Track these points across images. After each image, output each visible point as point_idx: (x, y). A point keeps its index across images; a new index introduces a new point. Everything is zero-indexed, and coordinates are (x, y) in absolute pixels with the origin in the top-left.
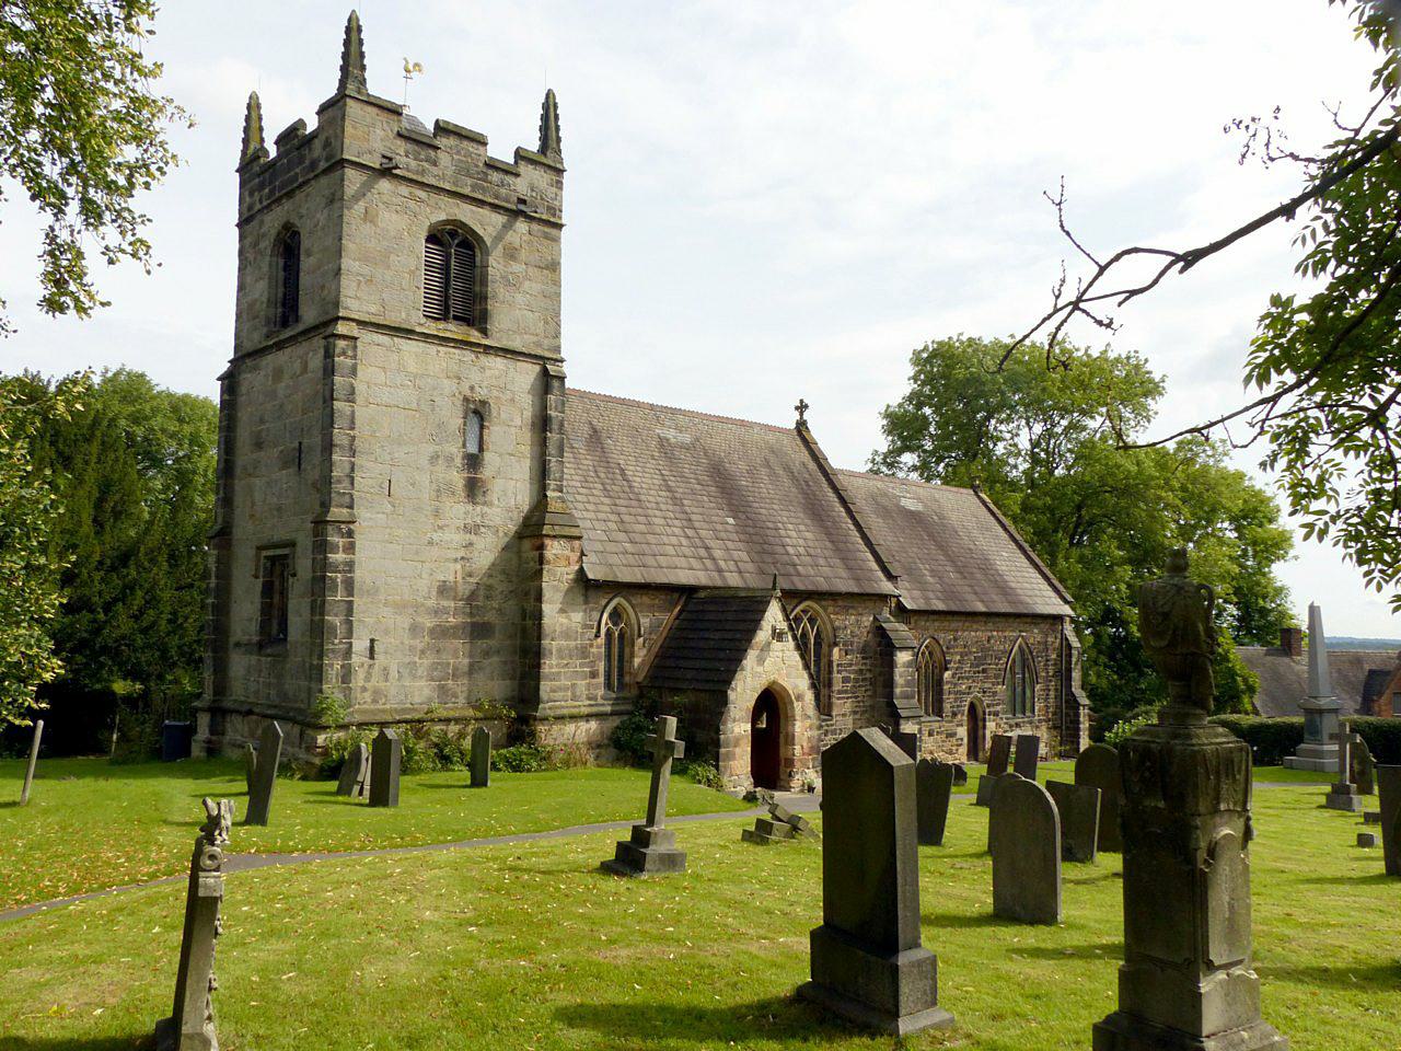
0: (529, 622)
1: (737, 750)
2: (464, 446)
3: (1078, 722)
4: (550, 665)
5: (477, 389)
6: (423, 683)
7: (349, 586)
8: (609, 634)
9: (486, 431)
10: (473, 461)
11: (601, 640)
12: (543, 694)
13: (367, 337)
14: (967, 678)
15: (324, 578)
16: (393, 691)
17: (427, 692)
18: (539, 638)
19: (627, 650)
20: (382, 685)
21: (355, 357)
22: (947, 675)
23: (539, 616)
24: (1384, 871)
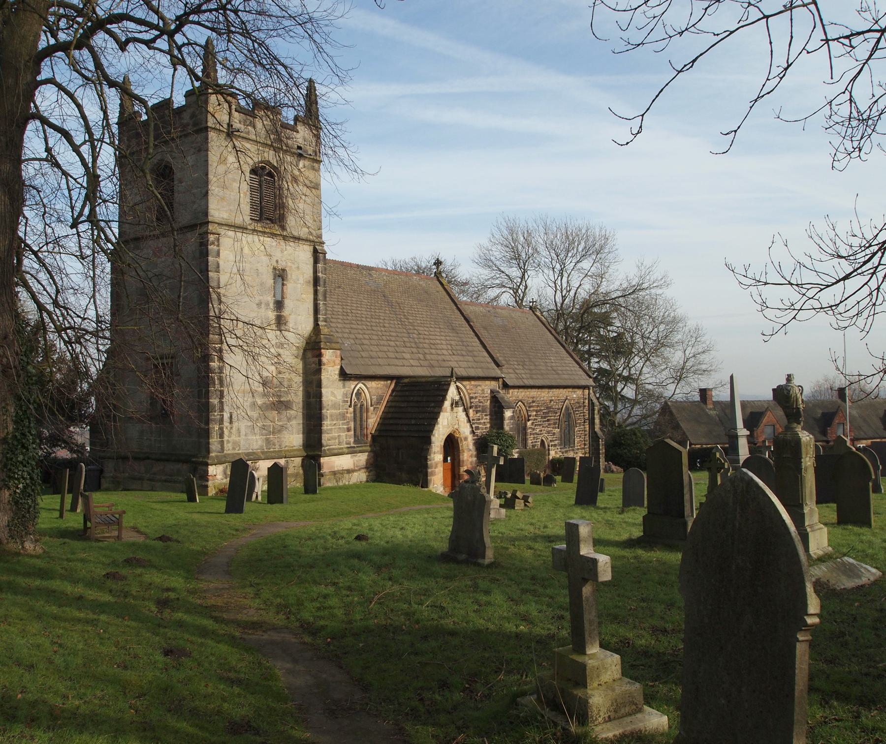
0: (312, 400)
1: (437, 470)
2: (274, 296)
3: (599, 449)
4: (327, 424)
5: (280, 262)
6: (258, 437)
7: (221, 381)
8: (355, 406)
9: (285, 287)
10: (279, 305)
11: (351, 409)
12: (324, 442)
13: (222, 231)
14: (540, 425)
15: (208, 376)
16: (242, 443)
17: (260, 443)
18: (321, 409)
19: (365, 415)
20: (237, 439)
21: (218, 246)
22: (529, 423)
23: (320, 395)
24: (771, 398)
